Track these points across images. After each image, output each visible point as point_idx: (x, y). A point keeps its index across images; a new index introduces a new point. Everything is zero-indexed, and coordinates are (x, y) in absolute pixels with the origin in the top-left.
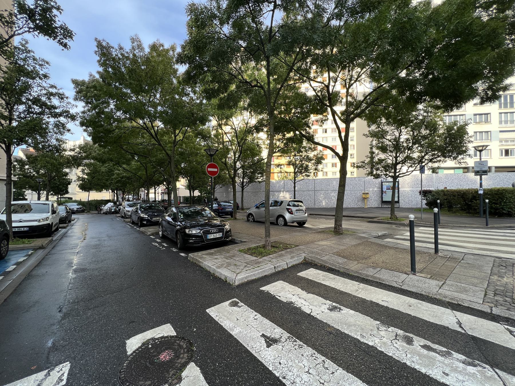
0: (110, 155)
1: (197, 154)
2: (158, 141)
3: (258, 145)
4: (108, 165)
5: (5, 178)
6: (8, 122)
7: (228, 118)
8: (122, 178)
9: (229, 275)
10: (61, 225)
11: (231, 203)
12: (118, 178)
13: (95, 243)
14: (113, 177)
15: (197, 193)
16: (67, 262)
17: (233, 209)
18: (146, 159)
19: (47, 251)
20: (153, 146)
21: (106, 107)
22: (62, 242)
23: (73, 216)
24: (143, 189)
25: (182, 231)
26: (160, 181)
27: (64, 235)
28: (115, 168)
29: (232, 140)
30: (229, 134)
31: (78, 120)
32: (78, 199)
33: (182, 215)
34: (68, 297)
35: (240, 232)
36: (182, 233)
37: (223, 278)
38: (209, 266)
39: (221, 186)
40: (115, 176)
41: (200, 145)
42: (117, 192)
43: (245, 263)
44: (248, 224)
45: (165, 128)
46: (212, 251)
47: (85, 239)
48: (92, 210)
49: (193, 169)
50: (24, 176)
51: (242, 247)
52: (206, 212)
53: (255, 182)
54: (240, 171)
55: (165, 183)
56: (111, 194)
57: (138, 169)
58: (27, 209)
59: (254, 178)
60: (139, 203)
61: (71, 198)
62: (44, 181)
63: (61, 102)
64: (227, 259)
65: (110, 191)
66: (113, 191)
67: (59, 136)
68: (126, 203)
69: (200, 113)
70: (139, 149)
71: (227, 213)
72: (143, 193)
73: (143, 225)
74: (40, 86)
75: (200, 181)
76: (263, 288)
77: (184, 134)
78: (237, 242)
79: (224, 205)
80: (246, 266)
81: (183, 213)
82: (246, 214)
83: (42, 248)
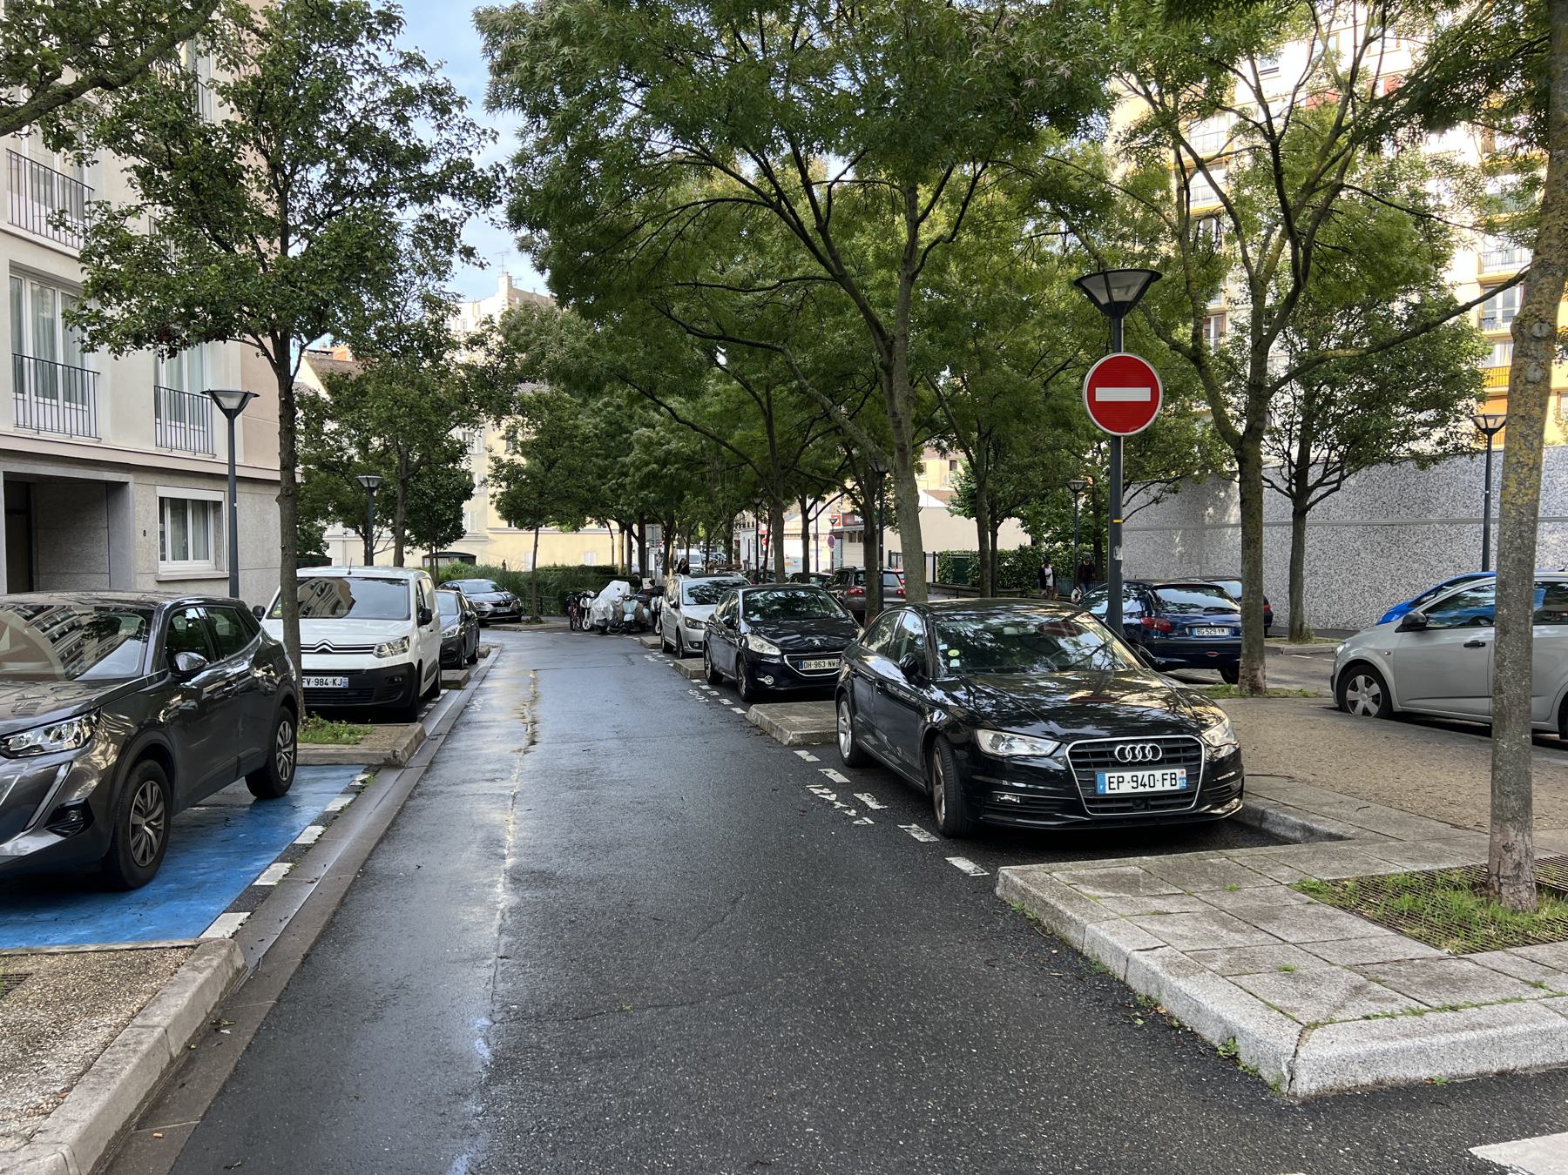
0: (619, 351)
1: (1020, 314)
2: (831, 259)
3: (1422, 216)
4: (606, 405)
5: (277, 477)
6: (277, 243)
7: (1218, 65)
8: (664, 463)
9: (1250, 1025)
10: (447, 675)
11: (1221, 593)
12: (647, 464)
13: (576, 760)
14: (628, 460)
15: (1012, 535)
16: (480, 835)
17: (1236, 632)
18: (769, 358)
19: (410, 775)
20: (801, 292)
21: (604, 122)
22: (456, 745)
23: (487, 638)
24: (749, 516)
25: (957, 738)
26: (824, 471)
27: (459, 720)
28: (631, 417)
29: (1242, 201)
30: (1219, 165)
31: (500, 202)
32: (495, 562)
33: (954, 653)
34: (501, 986)
35: (1298, 774)
36: (960, 747)
37: (1212, 1034)
38: (1118, 952)
39: (1154, 490)
40: (636, 454)
41: (1042, 260)
42: (641, 530)
43: (1350, 968)
44: (1342, 729)
45: (863, 183)
46: (1130, 870)
47: (533, 743)
48: (549, 615)
49: (1000, 401)
50: (323, 466)
51: (1321, 867)
52: (1082, 638)
53: (1391, 460)
54: (1285, 400)
55: (849, 484)
56: (617, 537)
57: (732, 416)
58: (337, 601)
59: (1379, 433)
60: (736, 585)
61: (470, 559)
62: (383, 486)
63: (440, 127)
64: (1224, 923)
65: (615, 525)
66: (625, 527)
67: (433, 285)
68: (679, 586)
69: (1055, 67)
70: (740, 310)
71: (1199, 656)
72: (748, 536)
73: (759, 695)
74: (372, 68)
75: (1031, 466)
76: (1480, 1152)
77: (965, 204)
78: (1279, 830)
79: (1183, 608)
80: (1358, 990)
81: (956, 640)
82: (1328, 667)
83: (392, 763)
